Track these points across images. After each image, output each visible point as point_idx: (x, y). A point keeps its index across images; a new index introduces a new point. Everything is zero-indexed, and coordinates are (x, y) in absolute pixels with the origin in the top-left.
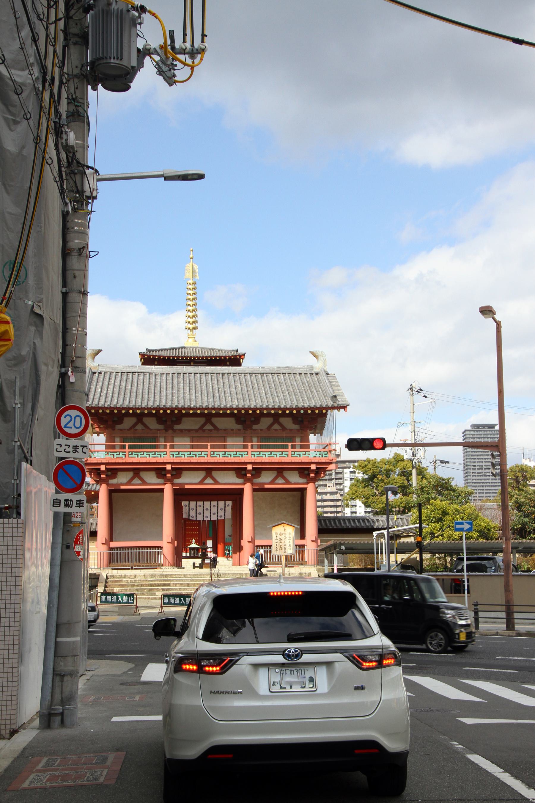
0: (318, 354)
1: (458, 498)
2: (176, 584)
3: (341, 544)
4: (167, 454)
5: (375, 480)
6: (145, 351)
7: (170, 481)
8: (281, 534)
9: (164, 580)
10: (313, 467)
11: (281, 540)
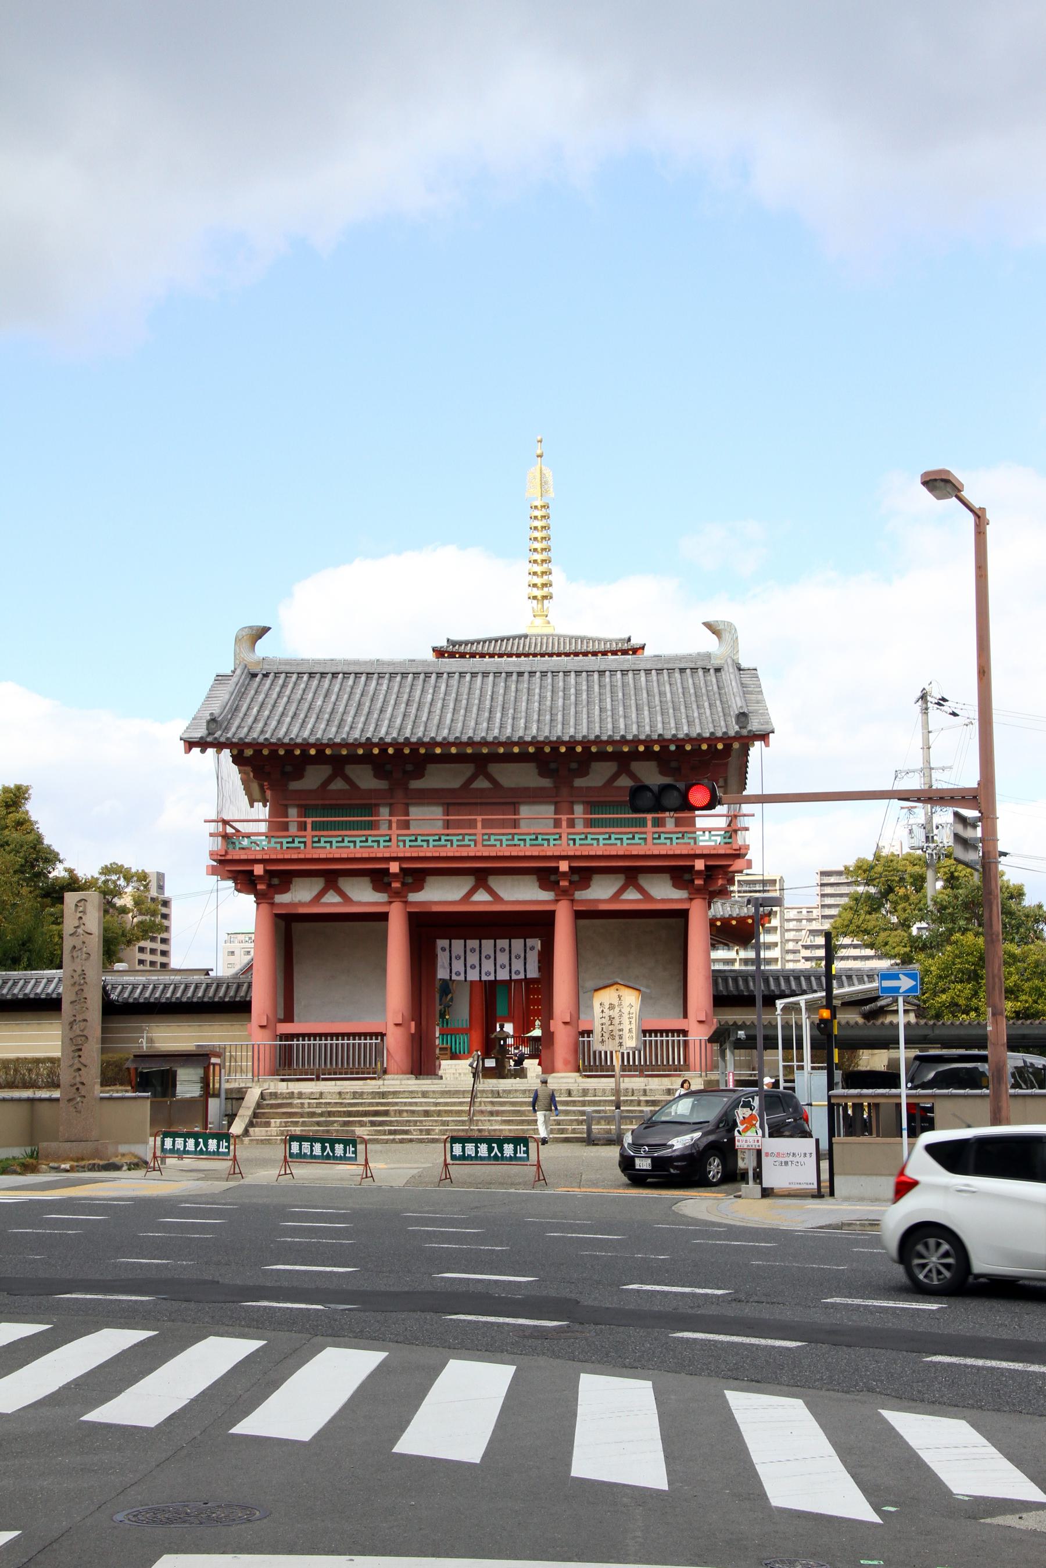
0: (721, 627)
1: (1018, 928)
2: (400, 1112)
3: (737, 1027)
4: (389, 839)
5: (891, 896)
6: (444, 643)
7: (399, 895)
8: (612, 1007)
9: (378, 1104)
10: (699, 865)
11: (611, 1018)
